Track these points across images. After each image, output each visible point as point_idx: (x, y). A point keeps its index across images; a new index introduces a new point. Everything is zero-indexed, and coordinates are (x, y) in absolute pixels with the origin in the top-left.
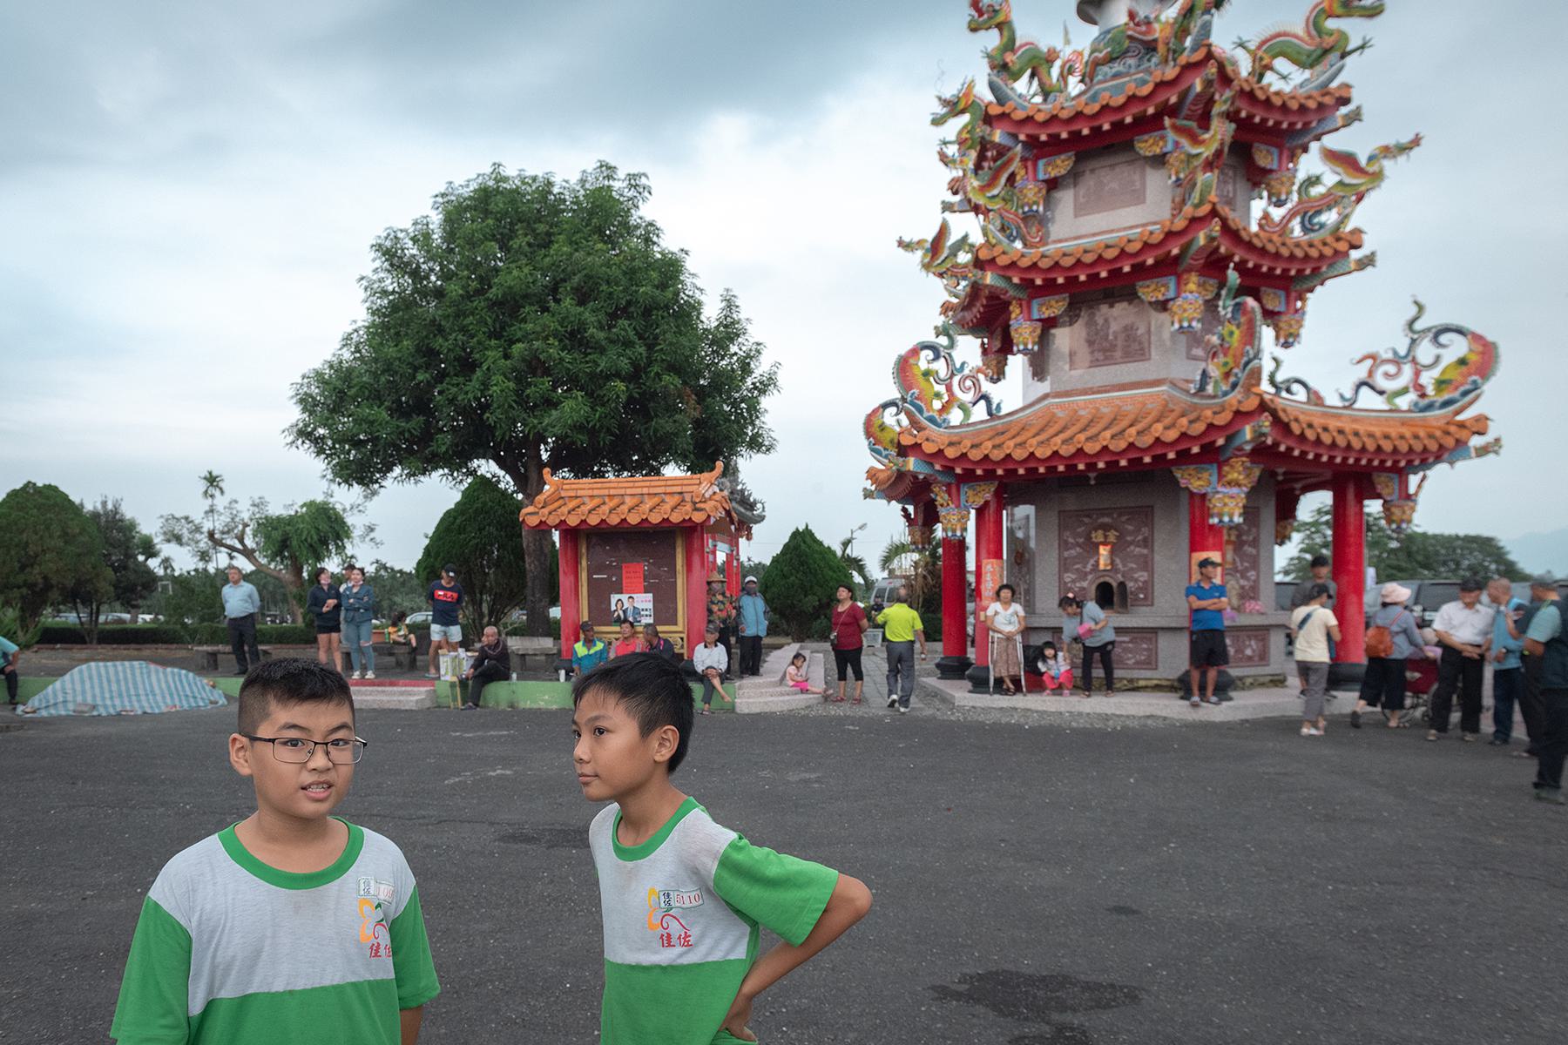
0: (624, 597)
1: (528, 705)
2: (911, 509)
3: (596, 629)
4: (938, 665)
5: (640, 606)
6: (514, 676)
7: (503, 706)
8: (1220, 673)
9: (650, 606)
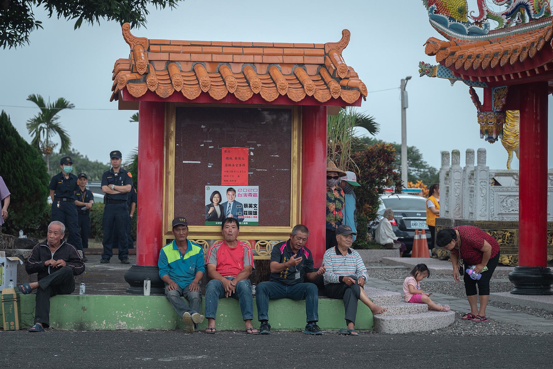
0: (222, 189)
1: (104, 325)
2: (480, 91)
3: (192, 228)
4: (513, 278)
5: (242, 200)
6: (83, 287)
7: (69, 327)
8: (183, 255)
9: (255, 200)
